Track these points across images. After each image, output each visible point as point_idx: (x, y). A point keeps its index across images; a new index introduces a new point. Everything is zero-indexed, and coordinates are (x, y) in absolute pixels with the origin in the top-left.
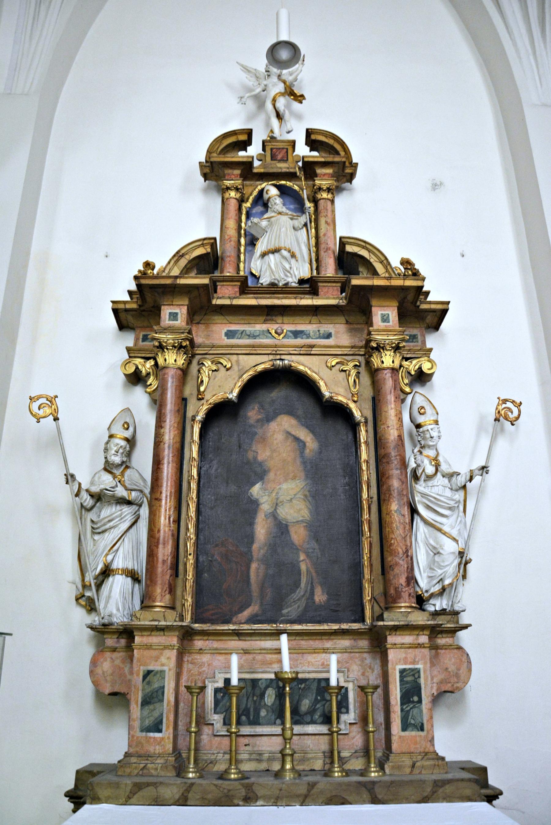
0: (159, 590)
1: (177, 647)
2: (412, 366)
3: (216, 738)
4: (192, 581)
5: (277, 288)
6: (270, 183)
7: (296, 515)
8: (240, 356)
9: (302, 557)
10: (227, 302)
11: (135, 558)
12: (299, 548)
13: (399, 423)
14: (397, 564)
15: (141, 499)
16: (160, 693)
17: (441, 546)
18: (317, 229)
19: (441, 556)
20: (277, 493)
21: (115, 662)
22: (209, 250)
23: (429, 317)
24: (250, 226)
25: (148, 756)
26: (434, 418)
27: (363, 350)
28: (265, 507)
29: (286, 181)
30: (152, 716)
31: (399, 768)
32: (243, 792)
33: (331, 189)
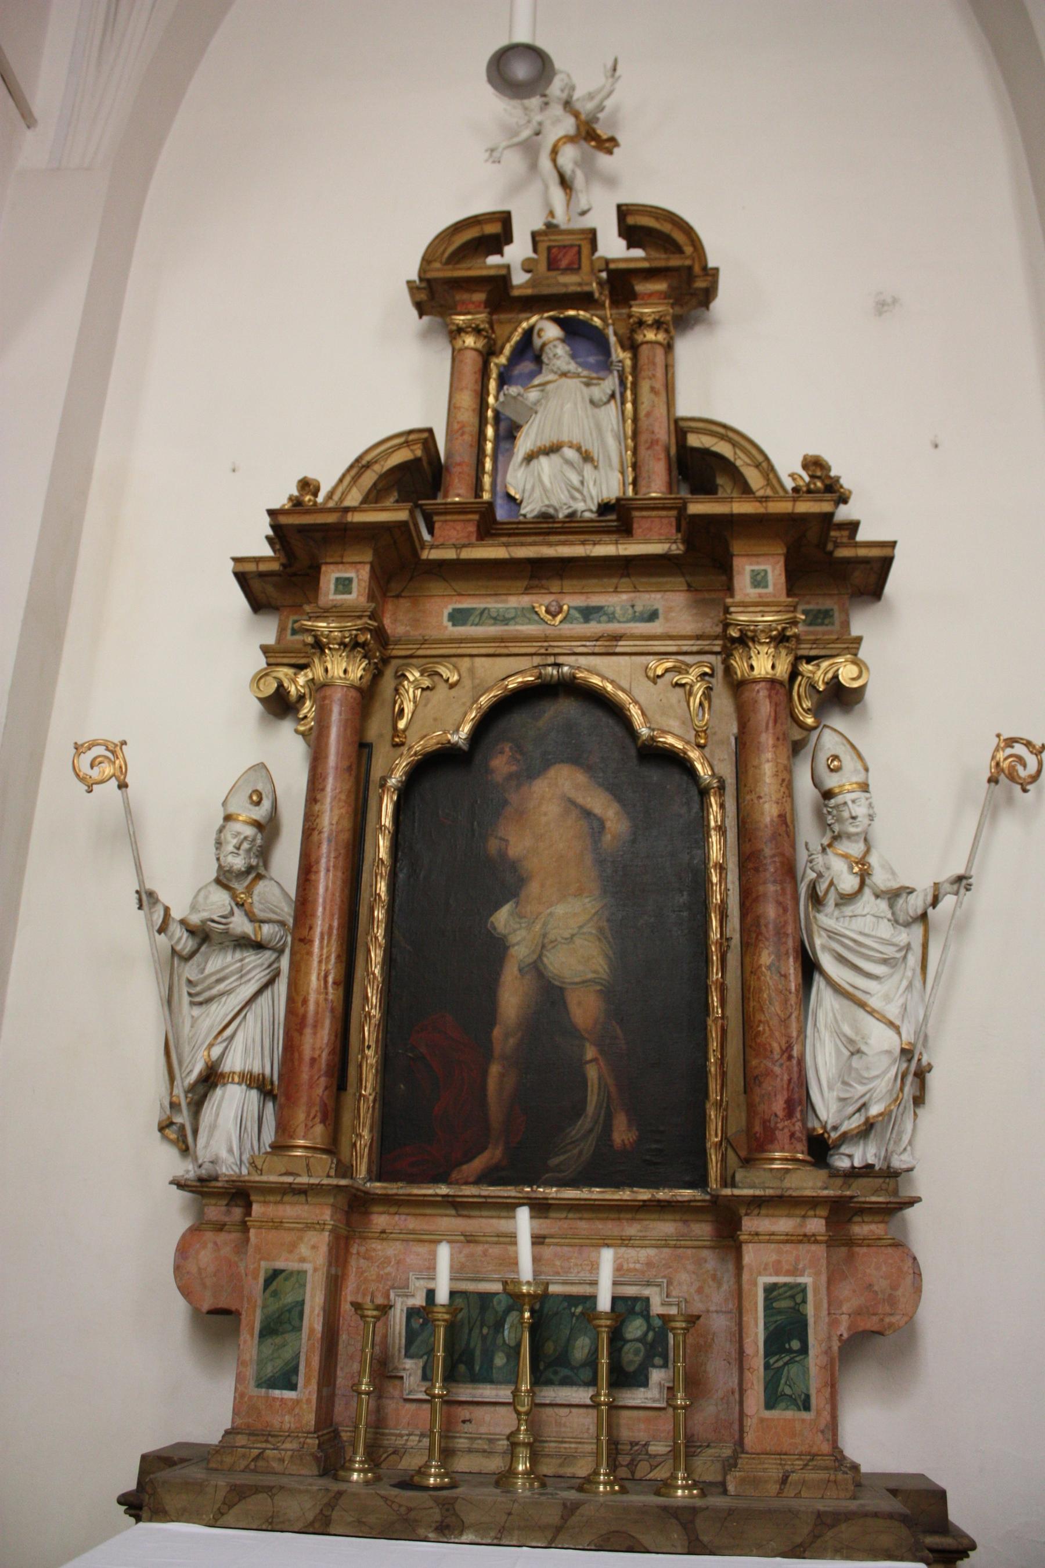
0: (301, 1116)
1: (330, 1227)
2: (819, 673)
3: (408, 1406)
4: (371, 1098)
5: (554, 522)
6: (546, 315)
7: (581, 968)
8: (477, 660)
9: (590, 1052)
10: (450, 554)
11: (267, 1052)
12: (586, 1036)
13: (782, 790)
14: (769, 1073)
15: (281, 938)
16: (295, 1313)
17: (863, 1038)
18: (635, 403)
19: (864, 1057)
20: (545, 924)
21: (222, 1252)
22: (419, 453)
23: (857, 574)
24: (503, 403)
25: (267, 1434)
26: (860, 778)
27: (720, 642)
28: (520, 951)
29: (578, 309)
30: (279, 1357)
31: (756, 1482)
32: (436, 1514)
33: (663, 323)
